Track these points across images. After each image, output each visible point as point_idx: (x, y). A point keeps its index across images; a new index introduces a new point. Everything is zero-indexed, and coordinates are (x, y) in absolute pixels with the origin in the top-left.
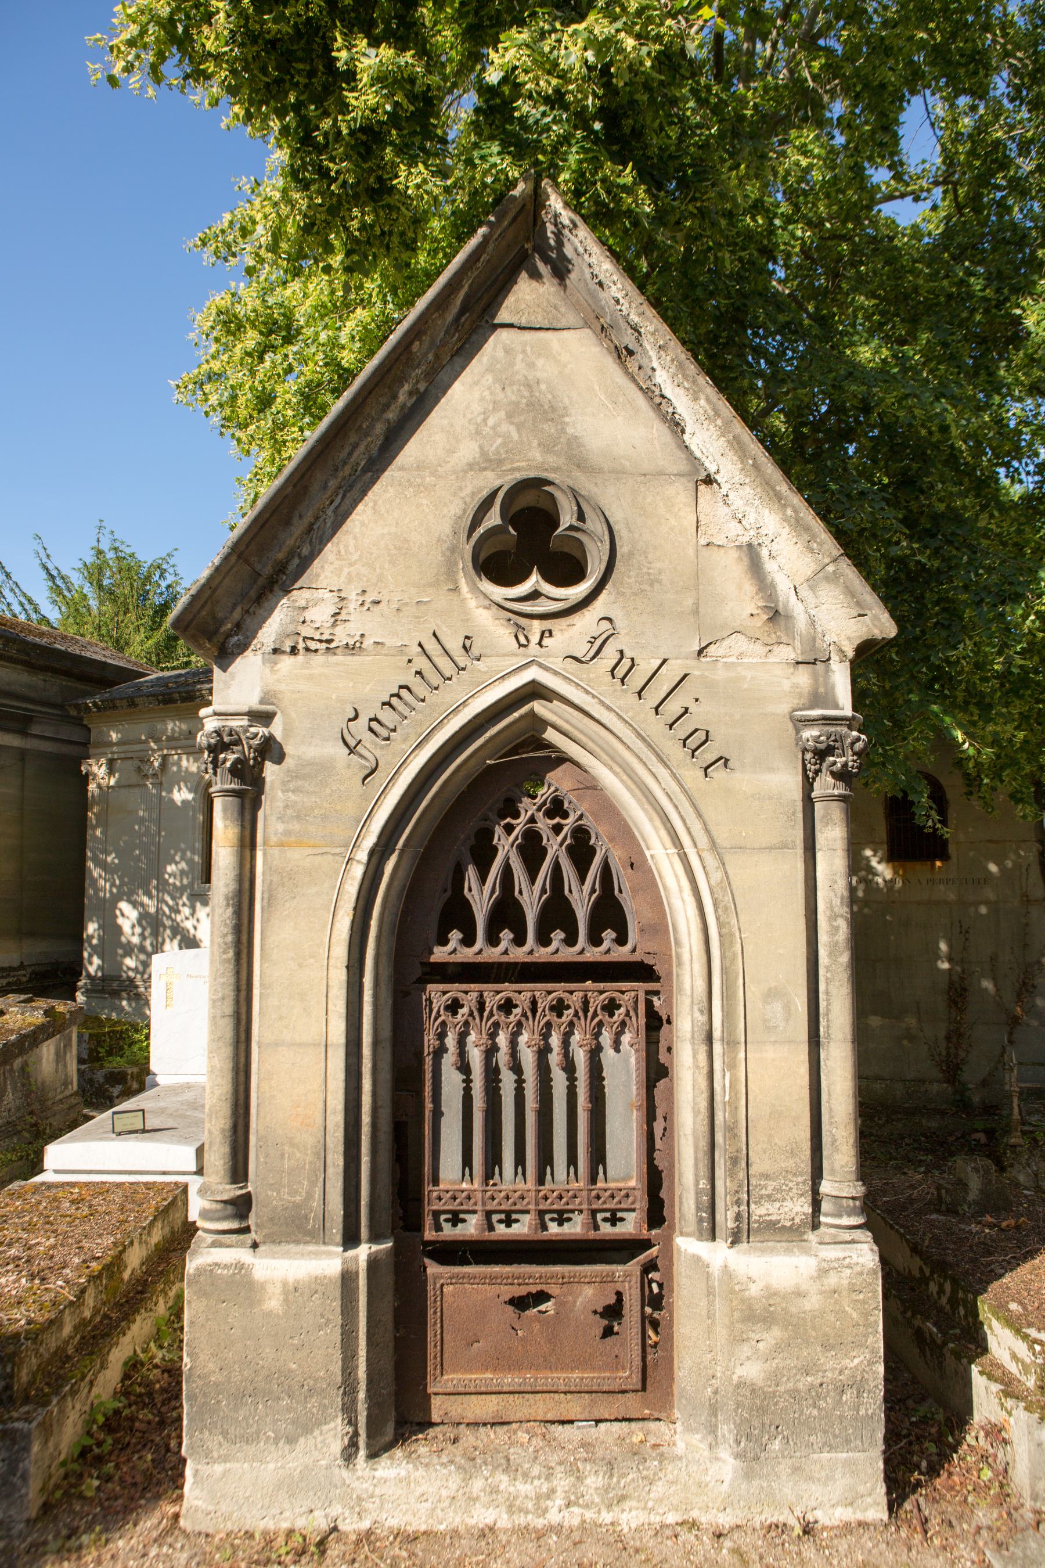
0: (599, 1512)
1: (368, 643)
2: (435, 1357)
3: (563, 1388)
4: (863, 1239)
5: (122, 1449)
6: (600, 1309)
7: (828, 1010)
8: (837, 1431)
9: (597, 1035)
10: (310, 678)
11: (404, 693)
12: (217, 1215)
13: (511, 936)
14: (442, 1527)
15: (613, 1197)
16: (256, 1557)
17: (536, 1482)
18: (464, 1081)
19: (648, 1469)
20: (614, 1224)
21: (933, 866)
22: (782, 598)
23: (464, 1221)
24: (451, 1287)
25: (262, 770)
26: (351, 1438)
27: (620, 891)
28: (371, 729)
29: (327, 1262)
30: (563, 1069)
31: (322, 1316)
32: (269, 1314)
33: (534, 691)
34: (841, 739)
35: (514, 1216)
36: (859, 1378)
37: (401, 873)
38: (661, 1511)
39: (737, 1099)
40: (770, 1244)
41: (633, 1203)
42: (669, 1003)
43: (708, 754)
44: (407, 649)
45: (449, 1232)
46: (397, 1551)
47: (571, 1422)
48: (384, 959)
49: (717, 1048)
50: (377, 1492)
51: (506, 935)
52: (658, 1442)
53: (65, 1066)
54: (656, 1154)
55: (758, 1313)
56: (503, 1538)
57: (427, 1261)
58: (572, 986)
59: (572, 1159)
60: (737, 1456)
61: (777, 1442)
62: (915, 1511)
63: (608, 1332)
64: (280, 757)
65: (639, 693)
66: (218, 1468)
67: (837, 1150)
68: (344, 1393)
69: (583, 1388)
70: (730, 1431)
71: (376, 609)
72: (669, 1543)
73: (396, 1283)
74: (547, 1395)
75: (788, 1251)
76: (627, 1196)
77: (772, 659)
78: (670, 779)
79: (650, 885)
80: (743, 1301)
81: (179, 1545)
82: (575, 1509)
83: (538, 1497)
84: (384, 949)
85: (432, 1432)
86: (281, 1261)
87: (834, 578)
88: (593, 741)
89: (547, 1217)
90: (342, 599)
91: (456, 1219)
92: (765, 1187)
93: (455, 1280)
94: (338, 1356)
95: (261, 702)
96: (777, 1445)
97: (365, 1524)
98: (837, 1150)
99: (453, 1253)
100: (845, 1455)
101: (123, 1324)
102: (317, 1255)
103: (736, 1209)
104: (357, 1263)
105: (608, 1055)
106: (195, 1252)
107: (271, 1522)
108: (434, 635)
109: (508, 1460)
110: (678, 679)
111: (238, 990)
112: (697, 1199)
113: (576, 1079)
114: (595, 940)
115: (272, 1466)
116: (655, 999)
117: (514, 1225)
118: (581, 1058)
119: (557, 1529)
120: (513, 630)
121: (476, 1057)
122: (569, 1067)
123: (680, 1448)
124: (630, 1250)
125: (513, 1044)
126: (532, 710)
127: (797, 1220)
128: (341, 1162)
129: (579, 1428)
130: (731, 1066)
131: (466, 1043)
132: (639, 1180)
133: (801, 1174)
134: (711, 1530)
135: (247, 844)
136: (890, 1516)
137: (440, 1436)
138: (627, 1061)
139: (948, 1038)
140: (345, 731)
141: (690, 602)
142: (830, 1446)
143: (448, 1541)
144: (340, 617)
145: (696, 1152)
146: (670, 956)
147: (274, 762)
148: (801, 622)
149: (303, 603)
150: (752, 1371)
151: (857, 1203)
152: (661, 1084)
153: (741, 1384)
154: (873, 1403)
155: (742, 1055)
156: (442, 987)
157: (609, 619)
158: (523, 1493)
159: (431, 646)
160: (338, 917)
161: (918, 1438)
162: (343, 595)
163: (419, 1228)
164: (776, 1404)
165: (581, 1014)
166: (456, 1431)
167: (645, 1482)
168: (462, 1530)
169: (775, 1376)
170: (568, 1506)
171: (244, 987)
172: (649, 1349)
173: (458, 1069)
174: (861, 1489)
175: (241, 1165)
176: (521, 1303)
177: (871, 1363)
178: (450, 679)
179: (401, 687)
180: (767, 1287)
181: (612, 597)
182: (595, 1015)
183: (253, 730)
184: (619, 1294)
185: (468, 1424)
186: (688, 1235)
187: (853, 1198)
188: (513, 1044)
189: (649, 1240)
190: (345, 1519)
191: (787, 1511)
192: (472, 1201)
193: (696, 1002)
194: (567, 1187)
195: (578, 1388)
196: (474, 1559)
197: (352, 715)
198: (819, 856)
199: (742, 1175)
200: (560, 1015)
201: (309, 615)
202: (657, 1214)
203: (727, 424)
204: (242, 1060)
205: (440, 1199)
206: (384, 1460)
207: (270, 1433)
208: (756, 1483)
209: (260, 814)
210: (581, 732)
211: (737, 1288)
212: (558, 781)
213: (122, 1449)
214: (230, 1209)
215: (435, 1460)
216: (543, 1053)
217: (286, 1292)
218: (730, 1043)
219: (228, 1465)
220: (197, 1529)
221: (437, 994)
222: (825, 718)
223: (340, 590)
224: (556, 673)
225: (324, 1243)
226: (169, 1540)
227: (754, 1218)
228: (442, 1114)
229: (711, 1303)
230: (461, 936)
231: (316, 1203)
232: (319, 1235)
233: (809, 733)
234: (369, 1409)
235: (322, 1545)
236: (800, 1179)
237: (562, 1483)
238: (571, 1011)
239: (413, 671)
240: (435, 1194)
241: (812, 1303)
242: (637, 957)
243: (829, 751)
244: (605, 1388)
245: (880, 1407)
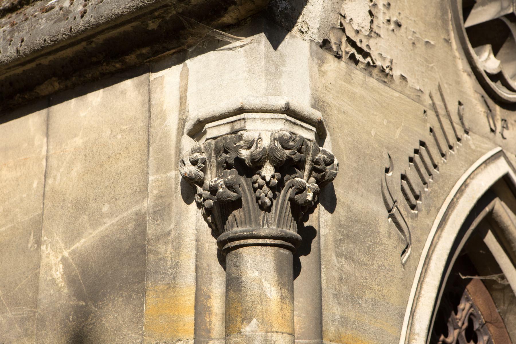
10: (353, 97)
147: (326, 208)
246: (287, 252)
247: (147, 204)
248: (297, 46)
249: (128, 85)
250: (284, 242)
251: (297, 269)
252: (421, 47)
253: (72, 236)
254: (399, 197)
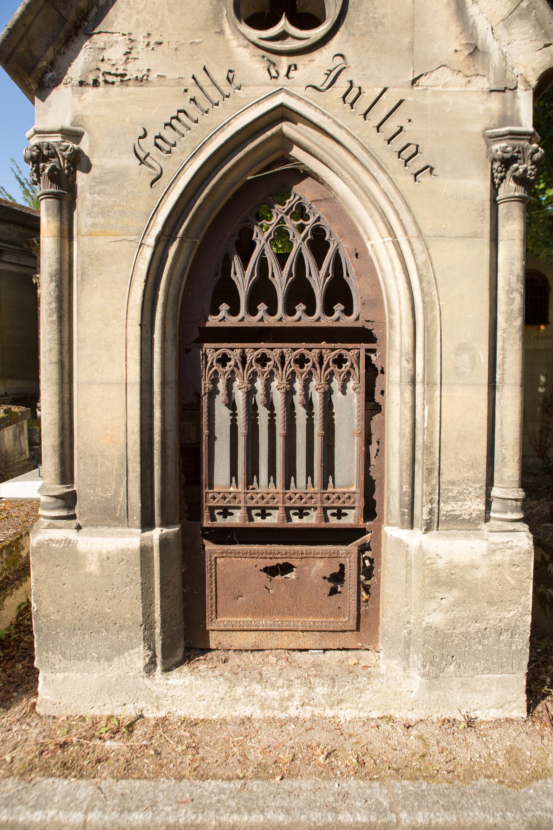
0: (324, 710)
1: (153, 76)
2: (212, 606)
3: (301, 628)
4: (522, 529)
5: (9, 660)
6: (328, 576)
7: (503, 362)
8: (495, 660)
9: (329, 381)
11: (182, 116)
12: (51, 506)
13: (266, 307)
14: (215, 717)
15: (339, 498)
16: (84, 734)
17: (280, 690)
18: (231, 415)
19: (359, 683)
20: (339, 518)
21: (539, 329)
22: (481, 37)
23: (232, 514)
24: (223, 559)
25: (75, 179)
26: (151, 659)
27: (348, 275)
28: (156, 145)
29: (129, 540)
30: (304, 406)
31: (127, 577)
32: (90, 575)
33: (283, 113)
34: (521, 151)
35: (268, 511)
36: (513, 625)
37: (182, 258)
38: (368, 710)
39: (434, 426)
40: (454, 531)
41: (354, 503)
42: (383, 358)
43: (417, 164)
44: (183, 81)
45: (220, 521)
46: (183, 733)
47: (307, 650)
48: (169, 323)
49: (419, 389)
50: (170, 693)
51: (262, 307)
52: (367, 664)
53: (20, 443)
54: (371, 469)
55: (443, 580)
56: (257, 725)
57: (205, 541)
58: (311, 345)
59: (310, 472)
60: (423, 675)
61: (452, 666)
62: (545, 711)
63: (333, 592)
64: (88, 168)
65: (365, 115)
66: (60, 676)
67: (506, 465)
68: (145, 629)
69: (315, 629)
70: (418, 659)
71: (159, 49)
72: (373, 731)
73: (183, 556)
74: (290, 632)
75: (466, 536)
76: (349, 498)
77: (470, 88)
78: (387, 182)
79: (370, 271)
80: (432, 571)
81: (34, 724)
82: (308, 708)
83: (282, 699)
84: (170, 315)
85: (209, 655)
86: (97, 539)
88: (328, 154)
89: (292, 512)
90: (132, 41)
91: (226, 513)
92: (452, 490)
93: (223, 555)
94: (139, 604)
95: (72, 125)
96: (451, 668)
97: (162, 714)
98: (506, 465)
99: (225, 536)
100: (499, 676)
101: (17, 582)
102: (123, 534)
103: (429, 506)
104: (152, 541)
105: (337, 396)
106: (36, 532)
107: (98, 711)
108: (205, 69)
109: (261, 675)
110: (395, 104)
111: (61, 344)
112: (401, 499)
113: (313, 414)
114: (329, 311)
115: (96, 675)
116: (372, 356)
117: (267, 518)
118: (317, 399)
119: (295, 720)
120: (266, 64)
121: (240, 397)
122: (309, 405)
123: (383, 668)
124: (350, 536)
125: (267, 388)
126: (281, 130)
127: (474, 515)
128: (138, 469)
129: (312, 654)
130: (429, 401)
131: (233, 389)
132: (358, 486)
133: (478, 482)
134: (403, 722)
135: (66, 235)
136: (528, 715)
137: (215, 658)
138: (351, 401)
139: (541, 432)
140: (137, 146)
141: (406, 41)
142: (490, 669)
143: (218, 726)
144: (130, 56)
145: (401, 465)
146: (384, 323)
147: (83, 172)
148: (495, 58)
149: (102, 45)
150: (437, 619)
151: (519, 504)
152: (376, 418)
153: (429, 628)
154: (522, 642)
155: (438, 393)
156: (214, 345)
157: (342, 56)
158: (271, 697)
159: (202, 78)
160: (133, 288)
161: (543, 663)
162: (132, 37)
163: (199, 518)
164: (453, 641)
165: (317, 366)
166: (226, 655)
167: (357, 691)
168: (229, 719)
169: (453, 624)
170: (303, 705)
171: (66, 342)
172: (362, 604)
173: (227, 405)
174: (509, 698)
175: (68, 471)
176: (272, 571)
177: (522, 615)
178: (217, 104)
179: (179, 111)
180: (451, 562)
181: (345, 38)
182: (328, 366)
183: (65, 144)
184: (342, 566)
185: (235, 650)
186: (393, 525)
187: (516, 500)
188: (267, 388)
189: (364, 529)
190: (148, 710)
191: (456, 711)
192: (237, 500)
193: (404, 354)
194: (306, 491)
195: (311, 629)
196: (236, 739)
197: (142, 133)
198: (501, 245)
199: (435, 481)
200: (302, 367)
201: (106, 55)
202: (370, 511)
204: (67, 396)
205: (214, 498)
206: (175, 673)
207: (94, 654)
208: (435, 693)
209: (75, 213)
210: (319, 146)
211: (428, 562)
212: (303, 191)
213: (9, 660)
214: (60, 502)
215: (211, 674)
216: (289, 394)
217: (101, 560)
218: (429, 383)
219: (66, 674)
220: (48, 713)
221: (211, 351)
222: (511, 133)
223: (130, 34)
224: (300, 99)
225: (128, 526)
226: (28, 720)
227: (442, 513)
228: (215, 438)
229: (408, 572)
230: (228, 307)
231: (122, 498)
232: (123, 521)
233: (498, 147)
234: (163, 639)
235: (131, 727)
236: (478, 486)
237: (299, 691)
238: (310, 364)
239: (189, 98)
240: (211, 495)
241: (482, 573)
242: (359, 324)
243: (513, 160)
244: (331, 629)
245: (526, 645)
246: (51, 200)
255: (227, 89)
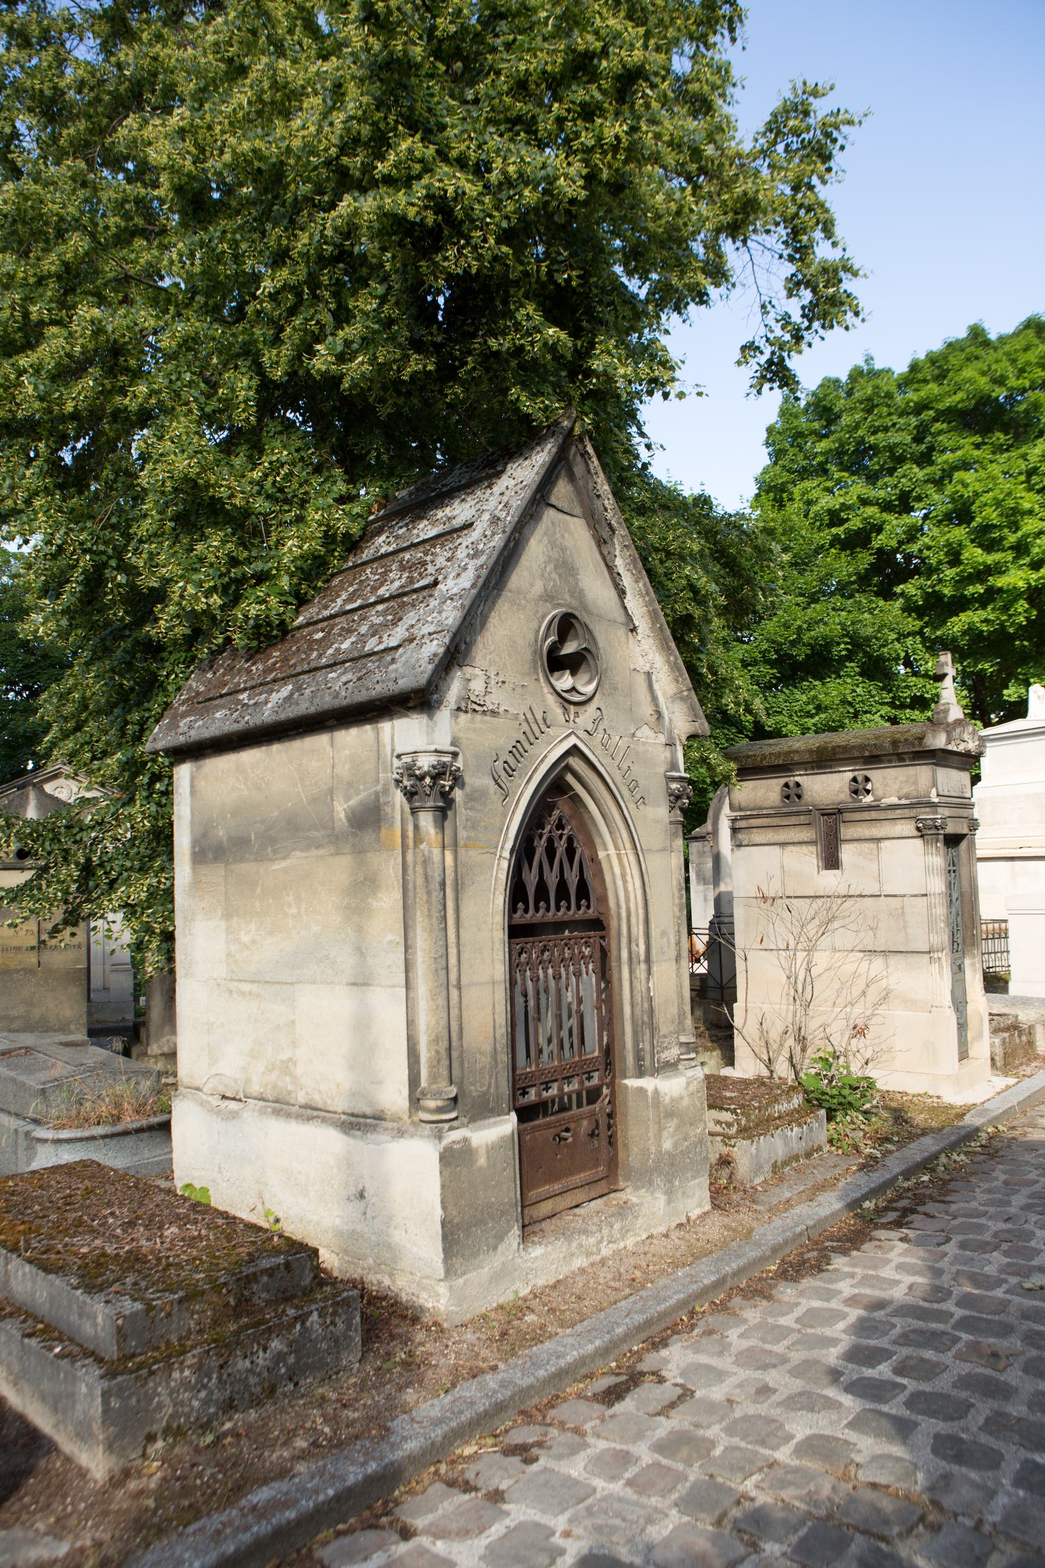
10: (475, 730)
11: (575, 762)
64: (462, 786)
66: (461, 1281)
87: (683, 699)
102: (495, 1124)
159: (529, 716)
203: (651, 601)
233: (674, 786)
247: (379, 787)
248: (444, 715)
249: (368, 728)
250: (437, 809)
251: (445, 817)
252: (519, 690)
253: (348, 798)
254: (503, 773)
255: (543, 728)
